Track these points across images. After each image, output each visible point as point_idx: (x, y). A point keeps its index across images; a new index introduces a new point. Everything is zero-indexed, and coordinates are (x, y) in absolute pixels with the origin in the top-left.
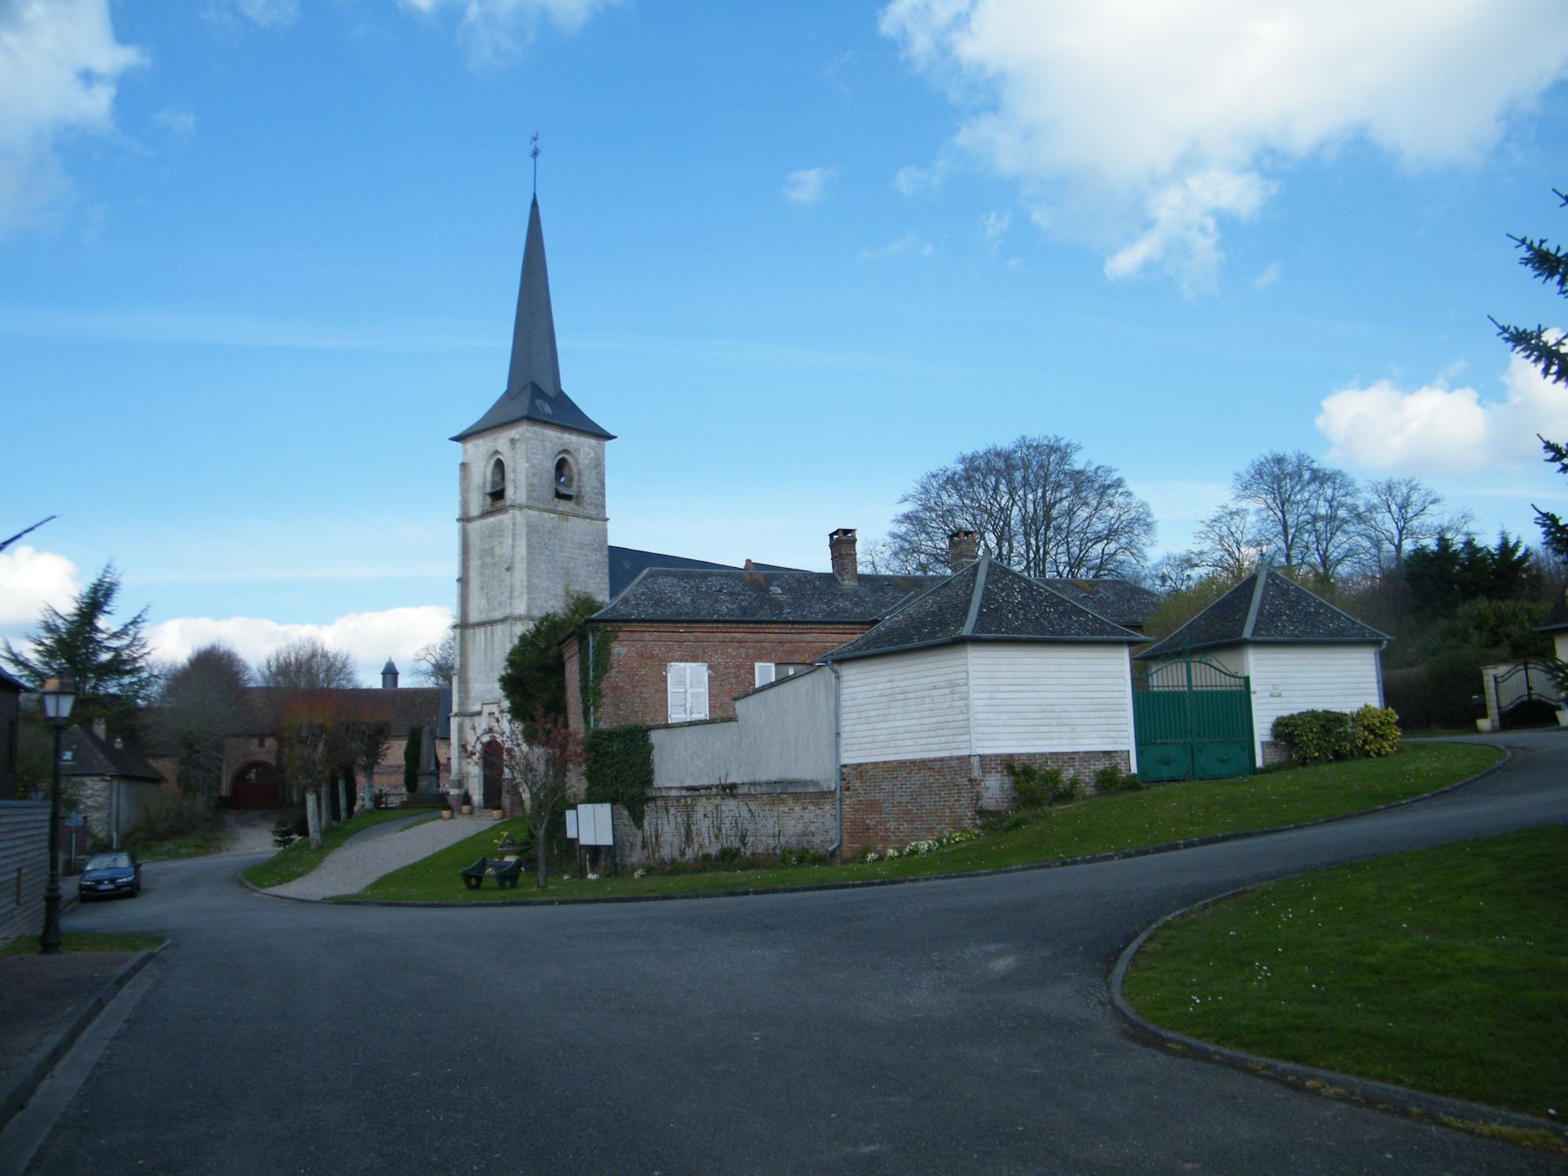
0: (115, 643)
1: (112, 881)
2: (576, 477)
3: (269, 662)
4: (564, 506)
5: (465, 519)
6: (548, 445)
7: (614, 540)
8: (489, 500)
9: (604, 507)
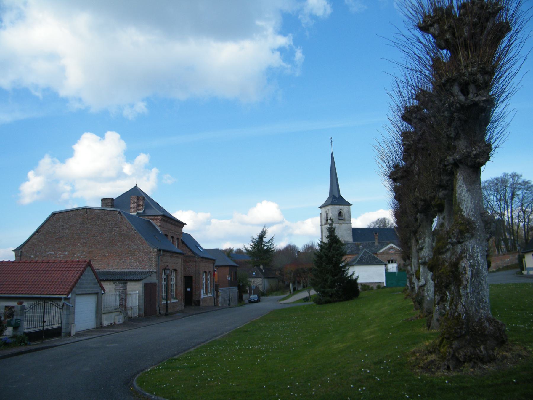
0: (267, 244)
1: (254, 300)
2: (343, 215)
3: (305, 246)
4: (341, 222)
5: (321, 225)
6: (336, 209)
7: (353, 226)
8: (326, 221)
9: (351, 221)
